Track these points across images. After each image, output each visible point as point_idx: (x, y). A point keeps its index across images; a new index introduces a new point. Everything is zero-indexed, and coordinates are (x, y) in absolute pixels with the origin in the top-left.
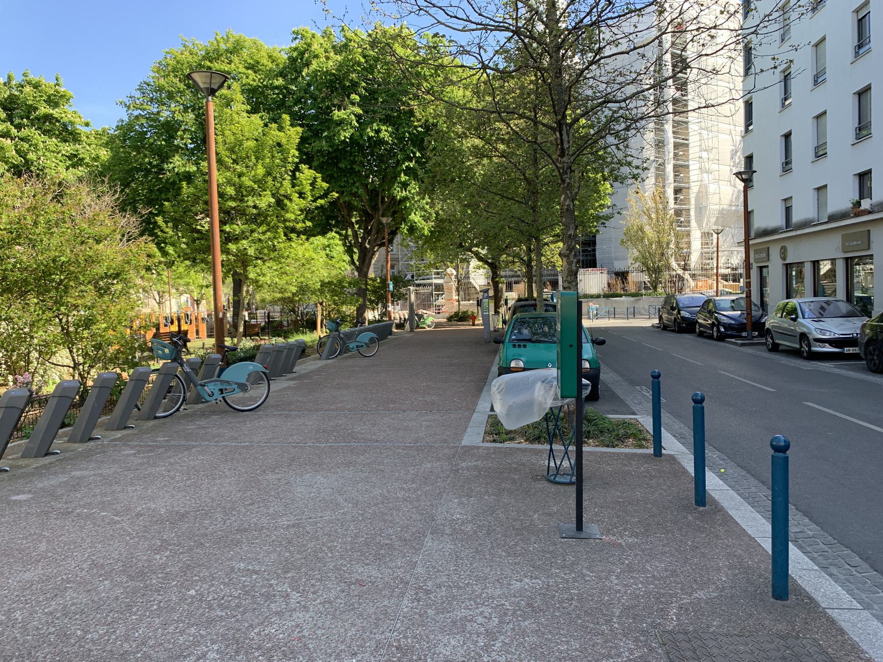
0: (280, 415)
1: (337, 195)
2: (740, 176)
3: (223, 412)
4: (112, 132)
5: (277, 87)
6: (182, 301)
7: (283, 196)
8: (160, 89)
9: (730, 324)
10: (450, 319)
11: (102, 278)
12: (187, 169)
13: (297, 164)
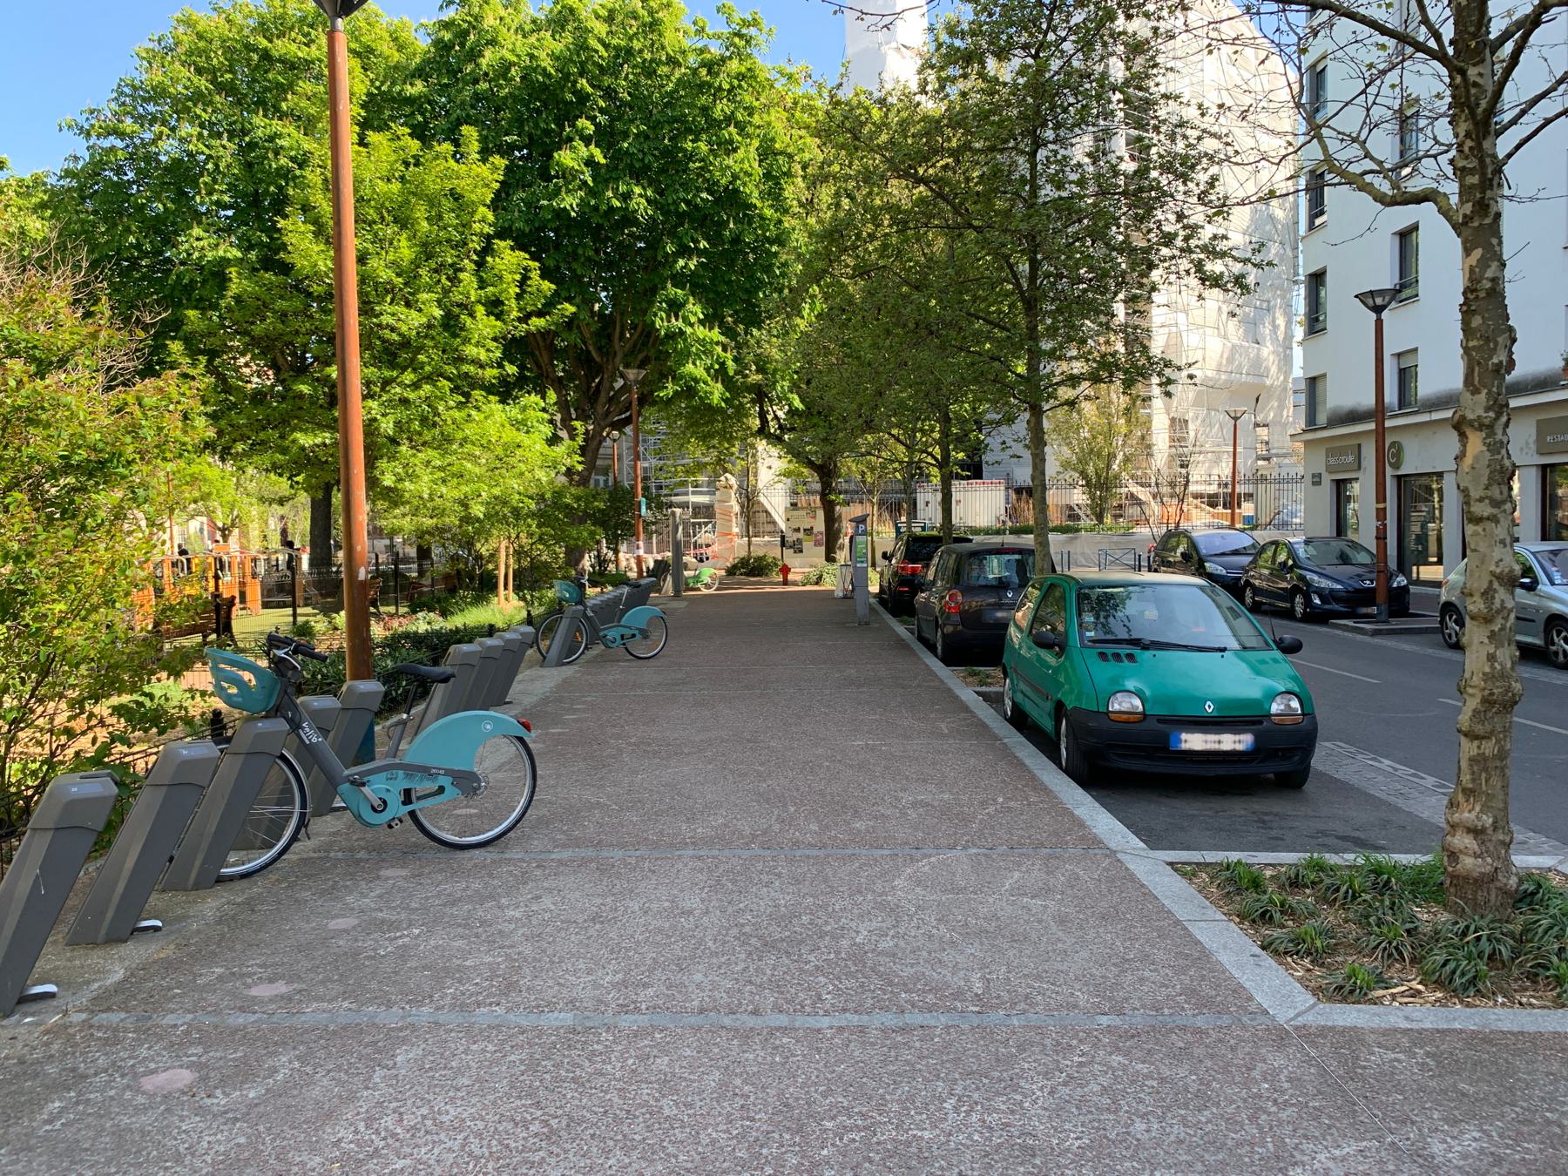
0: (584, 862)
1: (572, 309)
2: (1370, 302)
3: (406, 854)
4: (52, 180)
5: (410, 101)
6: (192, 531)
7: (459, 305)
8: (158, 94)
9: (1332, 590)
10: (731, 571)
11: (54, 474)
12: (221, 253)
13: (489, 238)
